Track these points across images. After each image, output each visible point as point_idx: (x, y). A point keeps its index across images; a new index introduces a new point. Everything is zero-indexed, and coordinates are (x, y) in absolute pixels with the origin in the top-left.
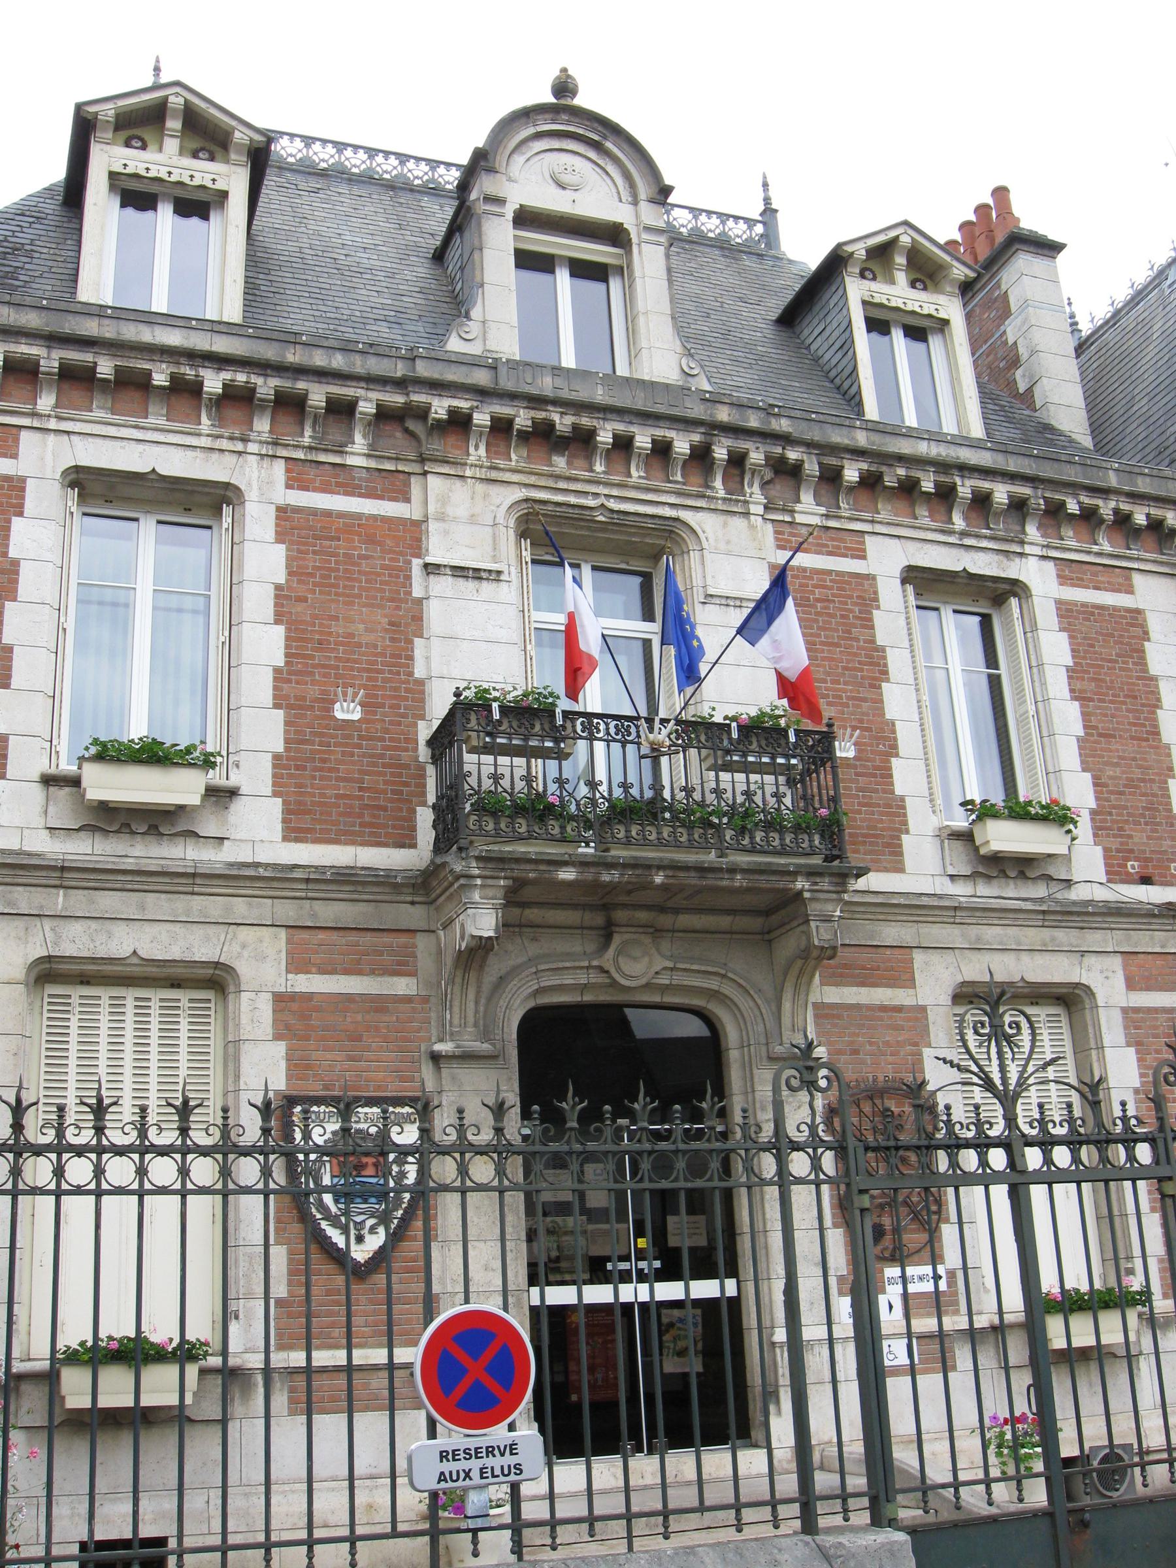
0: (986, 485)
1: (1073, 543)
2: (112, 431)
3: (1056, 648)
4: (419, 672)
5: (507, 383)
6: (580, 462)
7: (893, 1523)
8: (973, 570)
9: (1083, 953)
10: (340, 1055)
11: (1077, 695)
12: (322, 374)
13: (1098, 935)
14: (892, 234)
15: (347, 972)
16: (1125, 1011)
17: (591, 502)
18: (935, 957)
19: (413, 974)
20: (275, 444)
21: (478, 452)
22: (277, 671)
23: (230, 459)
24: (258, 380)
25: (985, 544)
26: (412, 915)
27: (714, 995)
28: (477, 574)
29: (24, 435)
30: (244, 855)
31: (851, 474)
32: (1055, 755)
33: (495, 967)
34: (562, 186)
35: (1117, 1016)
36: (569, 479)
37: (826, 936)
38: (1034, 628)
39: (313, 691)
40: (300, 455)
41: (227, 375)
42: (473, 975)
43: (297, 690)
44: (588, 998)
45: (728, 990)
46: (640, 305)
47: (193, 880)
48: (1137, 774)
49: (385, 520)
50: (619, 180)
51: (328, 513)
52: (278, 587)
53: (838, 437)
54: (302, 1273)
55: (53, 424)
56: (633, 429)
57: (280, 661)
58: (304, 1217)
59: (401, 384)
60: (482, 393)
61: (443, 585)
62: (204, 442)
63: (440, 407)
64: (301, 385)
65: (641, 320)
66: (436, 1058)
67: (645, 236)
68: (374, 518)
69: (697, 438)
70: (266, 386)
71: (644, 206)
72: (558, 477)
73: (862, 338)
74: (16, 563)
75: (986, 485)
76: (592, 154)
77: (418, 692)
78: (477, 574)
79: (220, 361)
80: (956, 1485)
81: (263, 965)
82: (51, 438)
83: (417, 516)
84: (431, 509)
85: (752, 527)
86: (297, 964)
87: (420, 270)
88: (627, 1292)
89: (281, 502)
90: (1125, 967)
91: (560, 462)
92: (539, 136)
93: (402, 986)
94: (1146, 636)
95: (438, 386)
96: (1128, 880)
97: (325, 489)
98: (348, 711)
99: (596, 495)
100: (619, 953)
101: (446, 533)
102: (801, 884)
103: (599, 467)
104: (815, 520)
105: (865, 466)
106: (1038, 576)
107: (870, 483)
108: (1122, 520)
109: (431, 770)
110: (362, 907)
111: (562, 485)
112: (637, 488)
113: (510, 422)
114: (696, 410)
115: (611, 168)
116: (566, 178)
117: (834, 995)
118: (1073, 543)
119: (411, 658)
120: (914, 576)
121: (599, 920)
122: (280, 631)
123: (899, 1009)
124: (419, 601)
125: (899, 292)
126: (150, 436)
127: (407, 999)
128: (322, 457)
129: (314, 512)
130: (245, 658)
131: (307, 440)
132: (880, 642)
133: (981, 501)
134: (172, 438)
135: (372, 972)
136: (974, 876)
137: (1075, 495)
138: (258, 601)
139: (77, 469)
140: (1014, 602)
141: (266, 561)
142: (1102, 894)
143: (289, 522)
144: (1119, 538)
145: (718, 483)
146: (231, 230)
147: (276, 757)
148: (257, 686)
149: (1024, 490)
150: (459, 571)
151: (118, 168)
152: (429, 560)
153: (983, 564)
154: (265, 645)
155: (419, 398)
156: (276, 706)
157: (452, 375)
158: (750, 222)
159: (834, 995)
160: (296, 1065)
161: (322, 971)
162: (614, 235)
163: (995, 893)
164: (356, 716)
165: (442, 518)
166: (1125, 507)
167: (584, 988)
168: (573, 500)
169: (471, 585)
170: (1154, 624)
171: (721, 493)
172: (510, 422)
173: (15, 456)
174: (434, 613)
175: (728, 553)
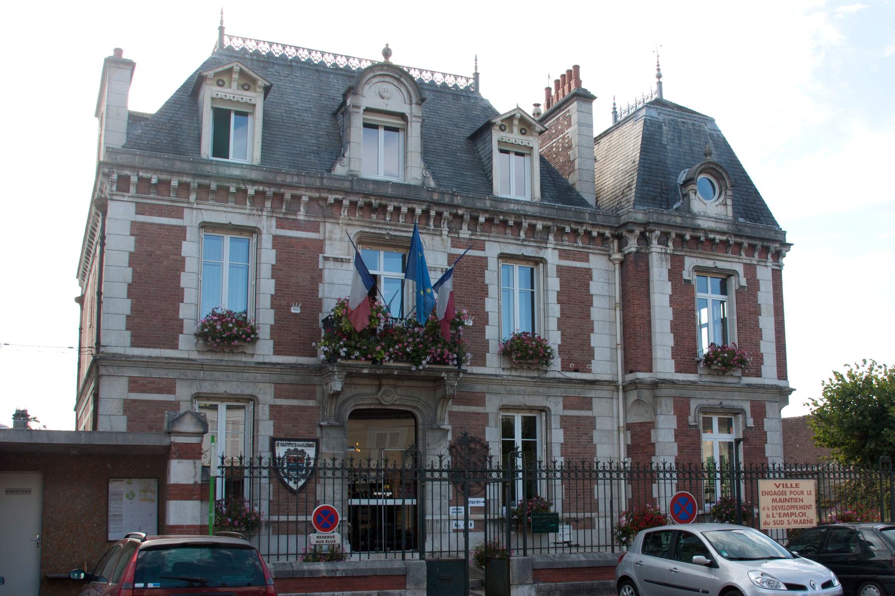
0: (534, 222)
1: (567, 243)
2: (216, 208)
3: (554, 284)
4: (320, 296)
5: (356, 188)
6: (381, 216)
7: (424, 559)
8: (526, 254)
9: (548, 396)
10: (290, 425)
11: (559, 302)
12: (290, 186)
13: (555, 390)
15: (293, 398)
16: (561, 416)
17: (384, 232)
18: (494, 396)
19: (315, 399)
20: (273, 212)
21: (344, 213)
22: (272, 296)
23: (257, 218)
24: (267, 189)
25: (532, 244)
26: (316, 380)
27: (415, 407)
28: (342, 260)
29: (185, 210)
30: (261, 360)
31: (482, 219)
32: (548, 324)
33: (341, 398)
34: (383, 98)
35: (558, 418)
36: (377, 223)
37: (451, 392)
38: (547, 276)
39: (284, 303)
40: (281, 216)
41: (256, 188)
42: (334, 401)
43: (279, 303)
44: (372, 407)
45: (415, 411)
46: (409, 149)
47: (244, 368)
48: (579, 331)
49: (310, 239)
50: (405, 94)
51: (290, 238)
52: (273, 265)
53: (479, 204)
54: (277, 492)
55: (195, 206)
56: (401, 205)
57: (273, 293)
58: (279, 475)
59: (318, 189)
60: (347, 193)
61: (330, 264)
62: (248, 211)
63: (331, 198)
64: (282, 190)
65: (409, 154)
66: (321, 426)
67: (413, 119)
68: (307, 239)
69: (424, 207)
70: (270, 191)
71: (414, 106)
72: (373, 223)
73: (497, 157)
74: (184, 258)
75: (534, 222)
76: (396, 83)
77: (318, 304)
78: (342, 260)
79: (254, 182)
80: (441, 552)
81: (267, 396)
82: (195, 211)
83: (322, 238)
84: (327, 236)
85: (443, 240)
86: (277, 395)
87: (326, 123)
88: (380, 502)
89: (274, 233)
90: (564, 401)
91: (374, 216)
92: (375, 76)
93: (311, 403)
94: (591, 279)
95: (331, 190)
96: (570, 370)
98: (295, 310)
99: (386, 229)
100: (383, 393)
101: (332, 245)
102: (443, 375)
103: (388, 218)
104: (467, 236)
105: (487, 216)
106: (551, 256)
107: (489, 221)
108: (588, 233)
109: (323, 330)
110: (298, 377)
111: (374, 225)
113: (356, 203)
114: (424, 195)
115: (403, 89)
116: (384, 95)
117: (456, 408)
118: (567, 243)
119: (318, 290)
120: (503, 257)
121: (377, 383)
122: (273, 281)
123: (479, 414)
124: (321, 270)
125: (514, 136)
126: (229, 210)
127: (313, 407)
128: (289, 217)
129: (286, 237)
130: (261, 291)
131: (284, 211)
132: (486, 282)
133: (532, 227)
134: (237, 210)
135: (301, 399)
136: (511, 369)
137: (569, 225)
138: (266, 271)
139: (204, 222)
140: (541, 265)
141: (269, 256)
142: (558, 375)
143: (277, 242)
144: (587, 241)
145: (432, 223)
146: (257, 121)
147: (271, 326)
148: (265, 301)
149: (550, 223)
150: (336, 260)
151: (214, 96)
152: (326, 255)
153: (529, 252)
154: (268, 286)
155: (324, 195)
156: (272, 308)
157: (337, 184)
158: (467, 79)
159: (456, 408)
160: (277, 428)
161: (285, 398)
162: (403, 116)
163: (518, 374)
164: (298, 312)
165: (330, 239)
166: (589, 229)
167: (371, 404)
168: (377, 231)
169: (339, 264)
170: (595, 275)
171: (432, 227)
172: (356, 203)
173: (182, 218)
174: (326, 274)
175: (433, 250)
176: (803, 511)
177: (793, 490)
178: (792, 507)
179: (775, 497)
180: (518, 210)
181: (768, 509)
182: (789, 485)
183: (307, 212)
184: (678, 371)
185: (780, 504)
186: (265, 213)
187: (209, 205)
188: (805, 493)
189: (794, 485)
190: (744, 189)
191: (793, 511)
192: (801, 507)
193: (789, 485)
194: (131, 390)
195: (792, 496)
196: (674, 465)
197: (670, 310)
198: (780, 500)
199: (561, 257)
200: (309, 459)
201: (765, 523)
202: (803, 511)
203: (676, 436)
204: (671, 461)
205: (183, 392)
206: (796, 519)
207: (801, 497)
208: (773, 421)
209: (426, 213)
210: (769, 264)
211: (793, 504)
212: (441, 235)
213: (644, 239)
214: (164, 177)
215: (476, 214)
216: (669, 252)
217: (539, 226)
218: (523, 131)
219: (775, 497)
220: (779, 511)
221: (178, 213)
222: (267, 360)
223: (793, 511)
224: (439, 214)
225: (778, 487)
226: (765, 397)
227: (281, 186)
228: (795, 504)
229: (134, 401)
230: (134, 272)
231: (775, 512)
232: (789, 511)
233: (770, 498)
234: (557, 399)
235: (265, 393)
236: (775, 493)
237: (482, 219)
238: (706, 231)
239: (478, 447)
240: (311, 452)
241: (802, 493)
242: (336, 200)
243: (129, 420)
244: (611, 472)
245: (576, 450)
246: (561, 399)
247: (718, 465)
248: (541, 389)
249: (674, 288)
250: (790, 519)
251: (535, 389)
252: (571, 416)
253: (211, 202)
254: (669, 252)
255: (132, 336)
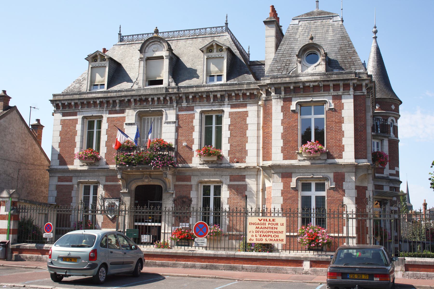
13: (225, 173)
14: (211, 44)
24: (103, 100)
30: (101, 167)
31: (191, 97)
41: (100, 100)
51: (114, 117)
62: (98, 110)
63: (126, 99)
72: (144, 106)
75: (216, 93)
92: (150, 43)
94: (248, 116)
97: (114, 113)
104: (186, 105)
107: (194, 97)
112: (156, 106)
123: (188, 185)
149: (224, 93)
166: (245, 92)
170: (250, 114)
176: (277, 234)
177: (270, 222)
178: (269, 232)
179: (258, 226)
180: (209, 89)
181: (253, 232)
182: (268, 220)
183: (119, 106)
184: (285, 158)
185: (261, 230)
186: (104, 109)
187: (86, 109)
188: (279, 224)
189: (271, 220)
190: (346, 52)
191: (269, 234)
192: (275, 232)
193: (268, 220)
194: (59, 181)
195: (270, 226)
196: (280, 209)
197: (282, 127)
198: (261, 228)
199: (63, 116)
200: (117, 206)
201: (250, 240)
202: (277, 234)
203: (282, 193)
204: (278, 207)
205: (75, 181)
206: (271, 238)
207: (276, 226)
208: (350, 184)
209: (165, 99)
210: (350, 93)
211: (270, 230)
212: (173, 107)
213: (268, 93)
214: (69, 102)
215: (188, 95)
216: (282, 97)
217: (219, 96)
218: (211, 51)
219: (258, 226)
220: (260, 234)
221: (75, 114)
222: (103, 167)
223: (269, 234)
224: (171, 98)
225: (260, 221)
226: (344, 170)
227: (109, 97)
228: (272, 230)
229: (59, 185)
230: (61, 138)
231: (257, 234)
232: (267, 234)
233: (255, 226)
234: (227, 177)
235: (102, 180)
236: (258, 224)
237: (191, 97)
238: (304, 83)
239: (187, 200)
240: (117, 204)
241: (277, 224)
242: (128, 100)
243: (57, 192)
244: (237, 213)
245: (235, 201)
246: (229, 177)
247: (261, 210)
248: (218, 173)
249: (284, 115)
250: (268, 238)
251: (215, 173)
252: (235, 185)
253: (86, 108)
254: (282, 97)
255: (60, 162)
